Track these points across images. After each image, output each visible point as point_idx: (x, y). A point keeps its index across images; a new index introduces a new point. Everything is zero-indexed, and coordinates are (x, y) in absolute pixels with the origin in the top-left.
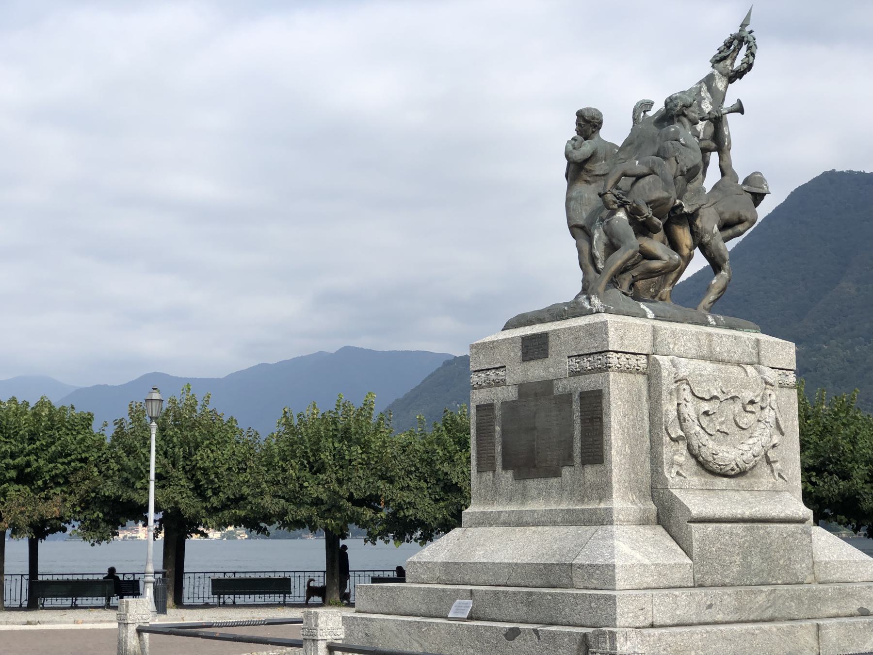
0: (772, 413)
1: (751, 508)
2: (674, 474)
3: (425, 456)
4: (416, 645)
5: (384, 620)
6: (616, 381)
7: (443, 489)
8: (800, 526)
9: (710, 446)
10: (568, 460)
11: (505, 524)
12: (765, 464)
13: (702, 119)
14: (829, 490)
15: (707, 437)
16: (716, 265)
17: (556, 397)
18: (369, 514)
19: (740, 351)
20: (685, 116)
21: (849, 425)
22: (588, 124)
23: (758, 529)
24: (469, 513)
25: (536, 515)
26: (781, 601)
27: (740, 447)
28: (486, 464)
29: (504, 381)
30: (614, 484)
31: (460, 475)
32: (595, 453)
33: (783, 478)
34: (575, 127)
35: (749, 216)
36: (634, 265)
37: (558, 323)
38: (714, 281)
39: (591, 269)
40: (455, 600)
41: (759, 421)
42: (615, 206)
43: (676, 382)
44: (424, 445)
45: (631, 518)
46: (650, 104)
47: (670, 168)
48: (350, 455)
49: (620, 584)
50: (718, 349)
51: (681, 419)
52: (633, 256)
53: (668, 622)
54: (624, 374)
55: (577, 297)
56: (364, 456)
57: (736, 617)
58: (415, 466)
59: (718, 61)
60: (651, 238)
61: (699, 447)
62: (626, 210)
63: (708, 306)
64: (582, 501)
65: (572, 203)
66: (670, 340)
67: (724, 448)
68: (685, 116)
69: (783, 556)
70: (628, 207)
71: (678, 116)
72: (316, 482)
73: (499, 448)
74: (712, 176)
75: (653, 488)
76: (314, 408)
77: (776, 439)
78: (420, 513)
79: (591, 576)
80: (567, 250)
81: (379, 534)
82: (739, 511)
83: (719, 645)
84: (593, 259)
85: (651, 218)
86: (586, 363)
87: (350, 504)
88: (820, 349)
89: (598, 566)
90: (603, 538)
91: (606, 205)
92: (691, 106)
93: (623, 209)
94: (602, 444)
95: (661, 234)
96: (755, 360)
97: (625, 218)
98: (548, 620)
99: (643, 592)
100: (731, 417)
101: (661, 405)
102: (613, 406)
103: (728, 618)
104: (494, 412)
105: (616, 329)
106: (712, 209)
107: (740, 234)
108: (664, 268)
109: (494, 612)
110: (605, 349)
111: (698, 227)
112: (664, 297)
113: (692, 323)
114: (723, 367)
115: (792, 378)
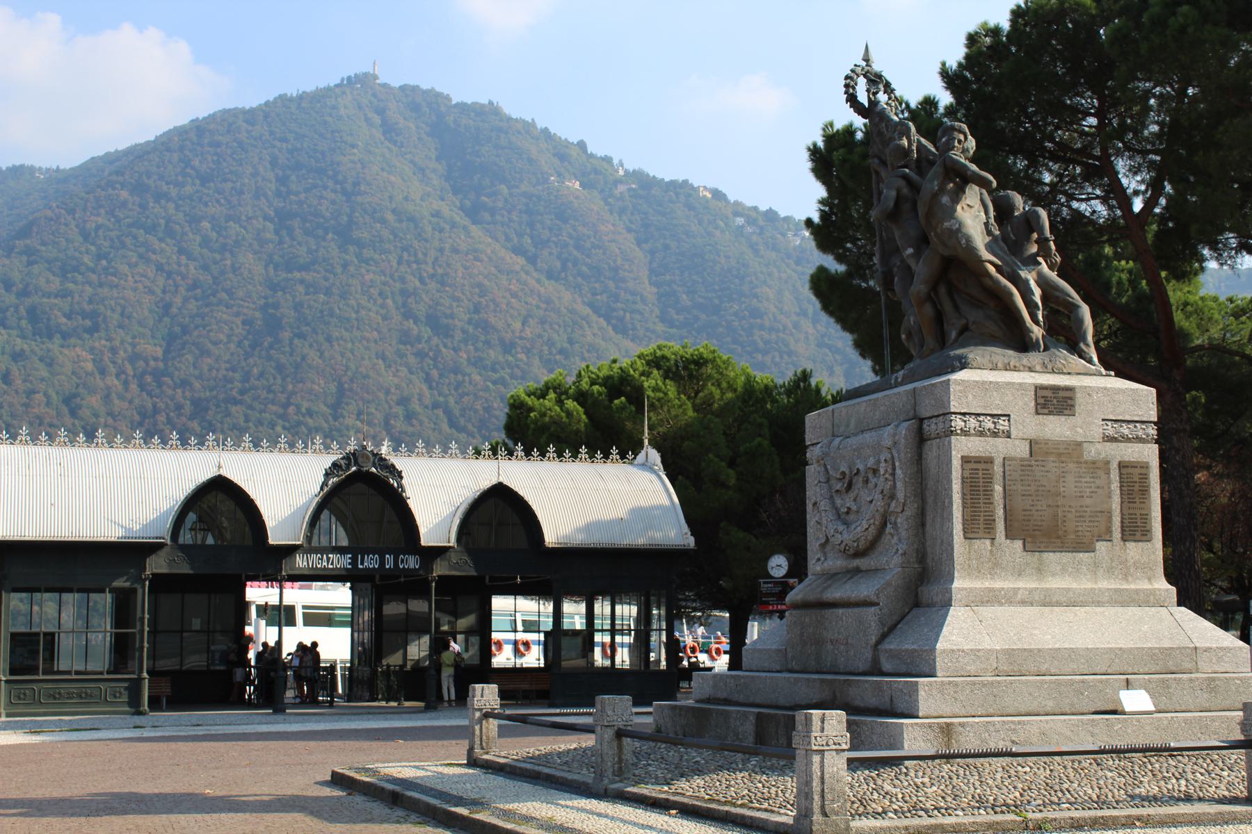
10: (1106, 536)
11: (1023, 603)
28: (978, 525)
79: (1220, 659)
86: (1125, 430)
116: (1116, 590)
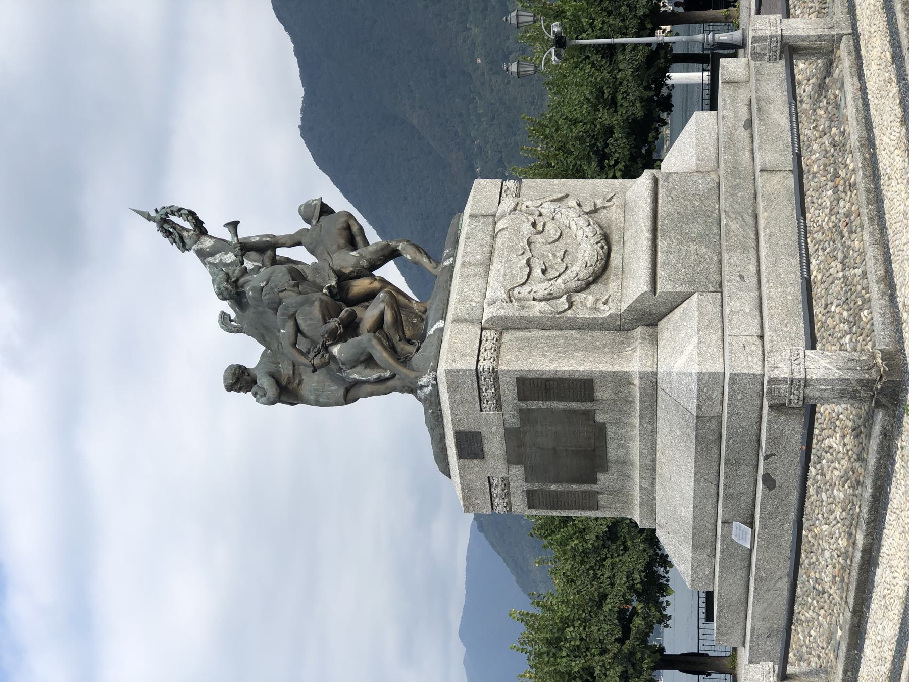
0: (545, 205)
1: (642, 232)
2: (606, 307)
3: (578, 559)
4: (779, 584)
5: (753, 617)
6: (509, 363)
7: (613, 541)
8: (660, 183)
9: (578, 269)
10: (589, 415)
11: (653, 483)
12: (597, 214)
13: (242, 263)
14: (623, 148)
15: (568, 272)
16: (392, 254)
17: (522, 426)
18: (638, 621)
19: (481, 234)
20: (237, 280)
21: (558, 125)
22: (240, 379)
23: (663, 225)
24: (641, 521)
25: (645, 451)
26: (737, 206)
27: (579, 239)
28: (590, 501)
29: (503, 479)
30: (615, 369)
31: (599, 523)
32: (582, 388)
33: (612, 197)
34: (242, 393)
35: (343, 220)
36: (388, 339)
37: (445, 421)
38: (408, 257)
39: (391, 383)
40: (732, 540)
41: (553, 219)
42: (327, 356)
43: (511, 301)
44: (566, 559)
45: (650, 353)
46: (224, 315)
47: (291, 298)
48: (575, 640)
49: (717, 368)
50: (479, 257)
51: (550, 298)
52: (379, 340)
53: (757, 320)
54: (501, 354)
55: (419, 399)
56: (577, 625)
57: (753, 252)
58: (588, 570)
59: (184, 246)
60: (361, 319)
61: (579, 280)
62: (331, 345)
63: (434, 264)
64: (632, 403)
65: (321, 400)
66: (468, 305)
67: (580, 255)
68: (237, 280)
69: (691, 201)
70: (328, 343)
71: (237, 287)
72: (603, 677)
73: (574, 487)
74: (301, 255)
75: (620, 329)
76: (524, 676)
77: (572, 203)
78: (639, 567)
79: (709, 397)
80: (373, 410)
81: (660, 612)
82: (645, 243)
83: (781, 271)
84: (380, 381)
85: (341, 319)
86: (489, 393)
87: (627, 642)
88: (480, 147)
89: (699, 390)
90: (670, 383)
91: (325, 365)
92: (227, 274)
93: (330, 348)
94: (574, 380)
95: (358, 310)
96: (491, 219)
97: (339, 346)
98: (754, 444)
99: (726, 345)
100: (549, 246)
101: (534, 317)
102: (533, 367)
103: (754, 260)
104: (536, 491)
105: (454, 361)
106: (335, 256)
107: (361, 229)
108: (393, 308)
109: (746, 499)
110: (474, 373)
111: (352, 272)
112: (423, 309)
113: (451, 281)
114: (496, 252)
115: (511, 184)
116: (641, 417)
